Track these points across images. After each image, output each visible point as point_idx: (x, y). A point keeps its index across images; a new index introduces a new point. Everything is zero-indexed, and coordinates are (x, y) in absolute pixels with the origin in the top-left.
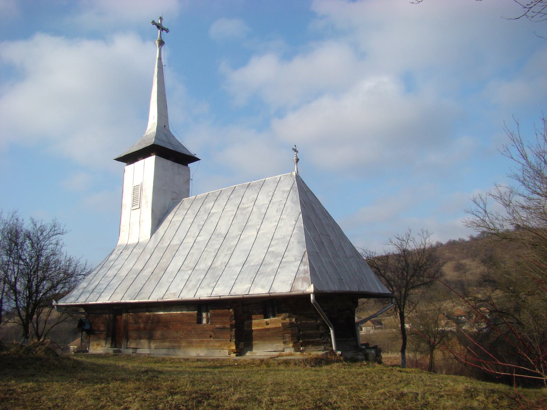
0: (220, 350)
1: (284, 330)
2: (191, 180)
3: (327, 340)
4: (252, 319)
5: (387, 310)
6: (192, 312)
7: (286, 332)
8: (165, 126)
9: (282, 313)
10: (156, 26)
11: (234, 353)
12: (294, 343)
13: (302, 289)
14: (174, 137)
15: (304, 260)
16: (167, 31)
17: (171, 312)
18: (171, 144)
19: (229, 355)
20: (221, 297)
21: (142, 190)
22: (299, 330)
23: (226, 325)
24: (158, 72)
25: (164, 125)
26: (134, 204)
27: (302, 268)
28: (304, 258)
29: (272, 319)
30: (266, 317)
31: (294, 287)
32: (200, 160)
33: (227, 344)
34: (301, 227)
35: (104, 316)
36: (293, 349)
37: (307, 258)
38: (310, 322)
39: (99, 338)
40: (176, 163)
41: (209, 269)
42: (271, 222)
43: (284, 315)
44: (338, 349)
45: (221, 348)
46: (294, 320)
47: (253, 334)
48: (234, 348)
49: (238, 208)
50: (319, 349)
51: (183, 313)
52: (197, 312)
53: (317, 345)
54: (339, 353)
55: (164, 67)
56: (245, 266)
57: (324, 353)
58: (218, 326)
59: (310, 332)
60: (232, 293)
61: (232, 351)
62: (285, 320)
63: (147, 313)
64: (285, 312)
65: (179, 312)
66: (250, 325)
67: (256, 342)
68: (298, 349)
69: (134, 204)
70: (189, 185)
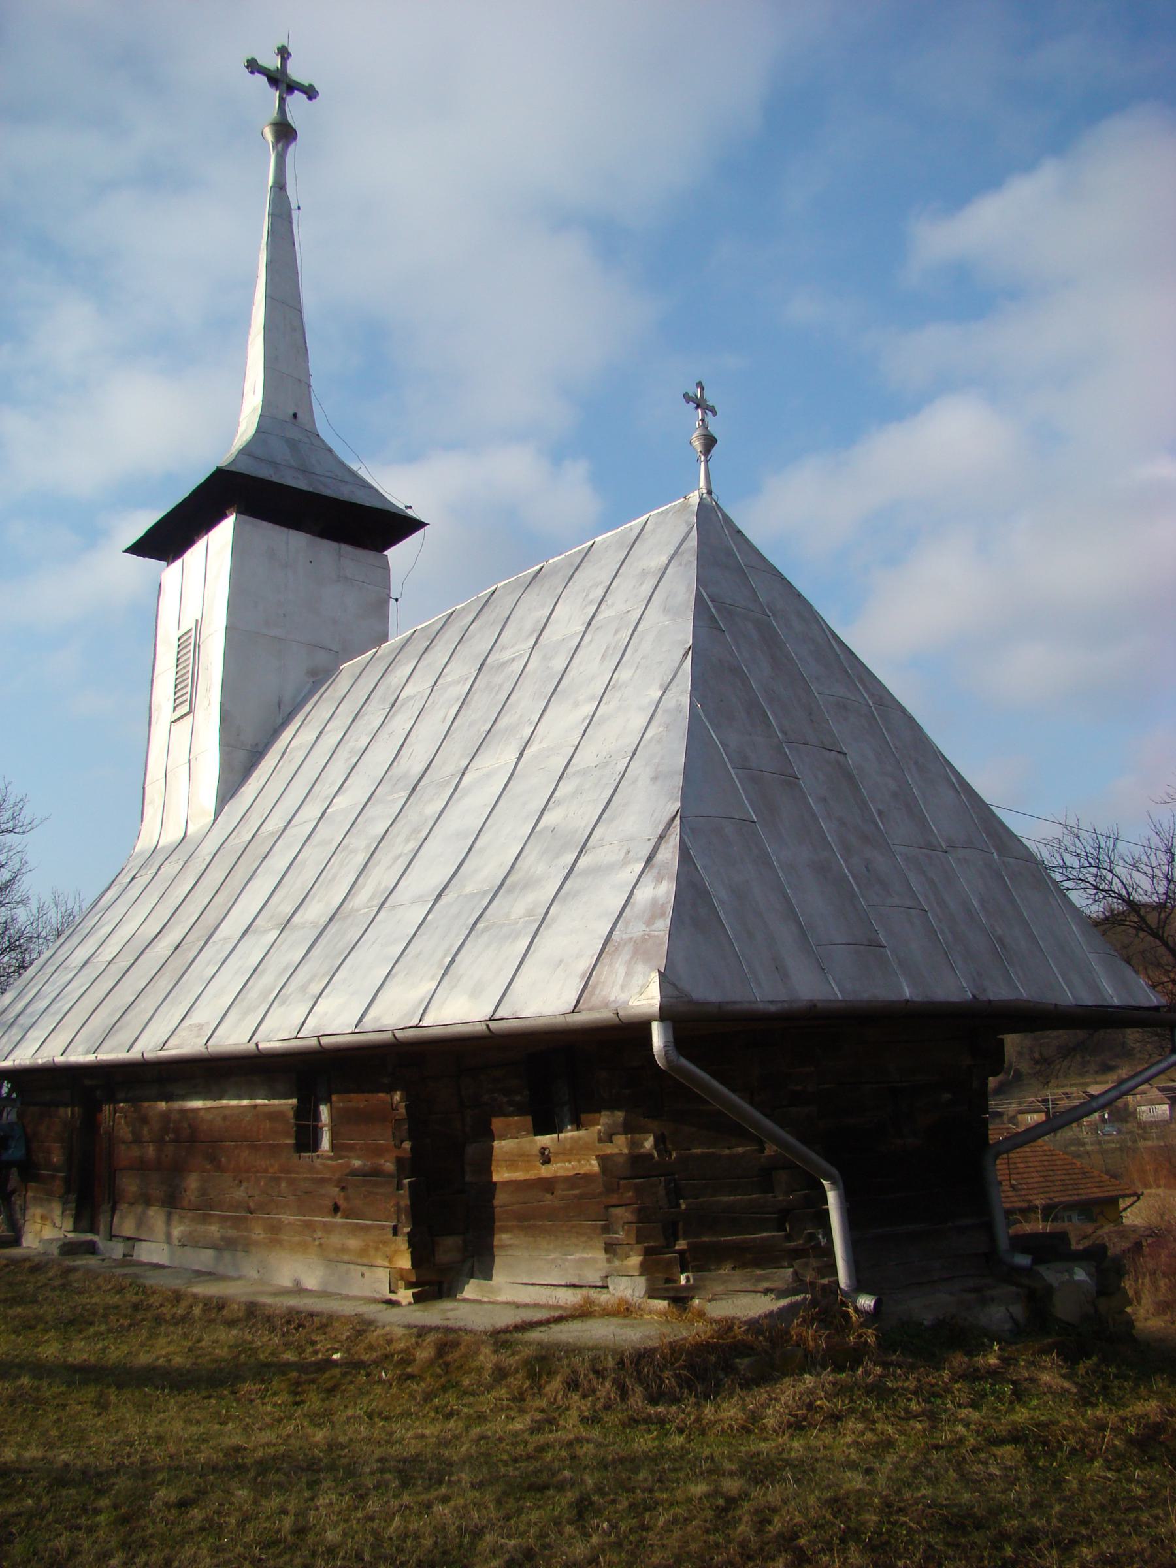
0: (364, 1269)
1: (610, 1189)
2: (392, 602)
3: (812, 1237)
4: (490, 1136)
5: (1132, 1077)
6: (282, 1101)
7: (614, 1199)
8: (295, 415)
9: (599, 1112)
10: (265, 79)
11: (410, 1285)
12: (648, 1252)
13: (623, 997)
14: (330, 451)
15: (661, 856)
16: (310, 93)
17: (225, 1102)
18: (305, 472)
19: (391, 1291)
20: (324, 1040)
21: (197, 646)
22: (675, 1193)
23: (382, 1161)
24: (272, 233)
25: (291, 412)
26: (178, 701)
27: (645, 894)
28: (663, 846)
29: (569, 1134)
30: (541, 1128)
31: (595, 988)
32: (427, 524)
33: (385, 1243)
34: (679, 708)
35: (62, 1110)
36: (641, 1283)
37: (674, 847)
38: (727, 1152)
39: (50, 1194)
40: (265, 524)
41: (331, 919)
42: (576, 704)
43: (605, 1120)
44: (860, 1285)
45: (365, 1261)
46: (649, 1143)
47: (496, 1202)
48: (405, 1262)
49: (480, 669)
50: (766, 1285)
51: (256, 1106)
52: (294, 1101)
53: (758, 1263)
54: (866, 1302)
55: (294, 214)
56: (444, 900)
57: (781, 1310)
58: (357, 1163)
59: (725, 1199)
60: (368, 1024)
61: (402, 1278)
62: (611, 1142)
63: (162, 1105)
64: (612, 1107)
65: (245, 1102)
66: (485, 1162)
67: (505, 1236)
68: (668, 1281)
69: (178, 701)
70: (385, 618)
